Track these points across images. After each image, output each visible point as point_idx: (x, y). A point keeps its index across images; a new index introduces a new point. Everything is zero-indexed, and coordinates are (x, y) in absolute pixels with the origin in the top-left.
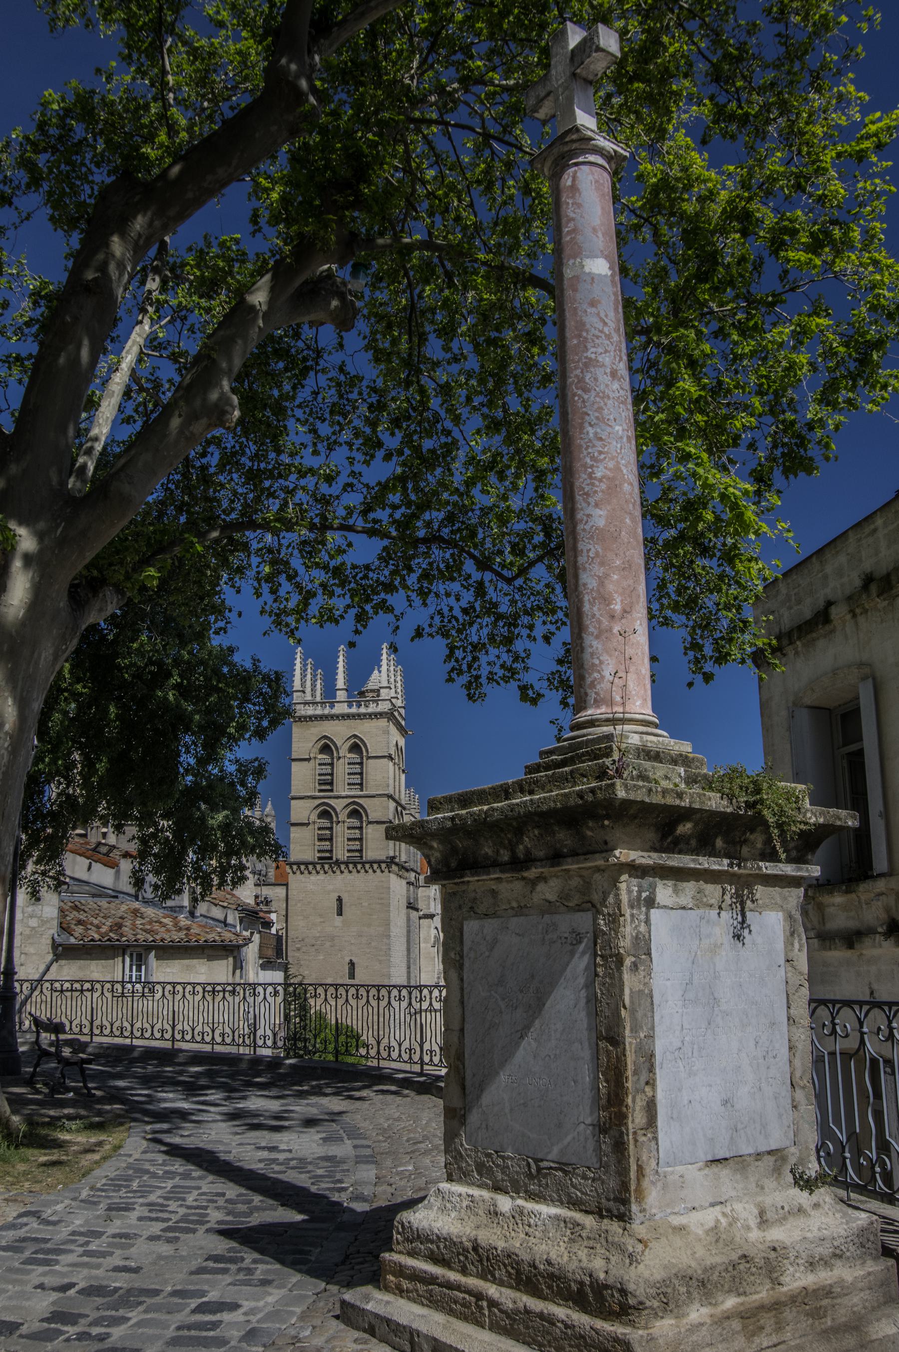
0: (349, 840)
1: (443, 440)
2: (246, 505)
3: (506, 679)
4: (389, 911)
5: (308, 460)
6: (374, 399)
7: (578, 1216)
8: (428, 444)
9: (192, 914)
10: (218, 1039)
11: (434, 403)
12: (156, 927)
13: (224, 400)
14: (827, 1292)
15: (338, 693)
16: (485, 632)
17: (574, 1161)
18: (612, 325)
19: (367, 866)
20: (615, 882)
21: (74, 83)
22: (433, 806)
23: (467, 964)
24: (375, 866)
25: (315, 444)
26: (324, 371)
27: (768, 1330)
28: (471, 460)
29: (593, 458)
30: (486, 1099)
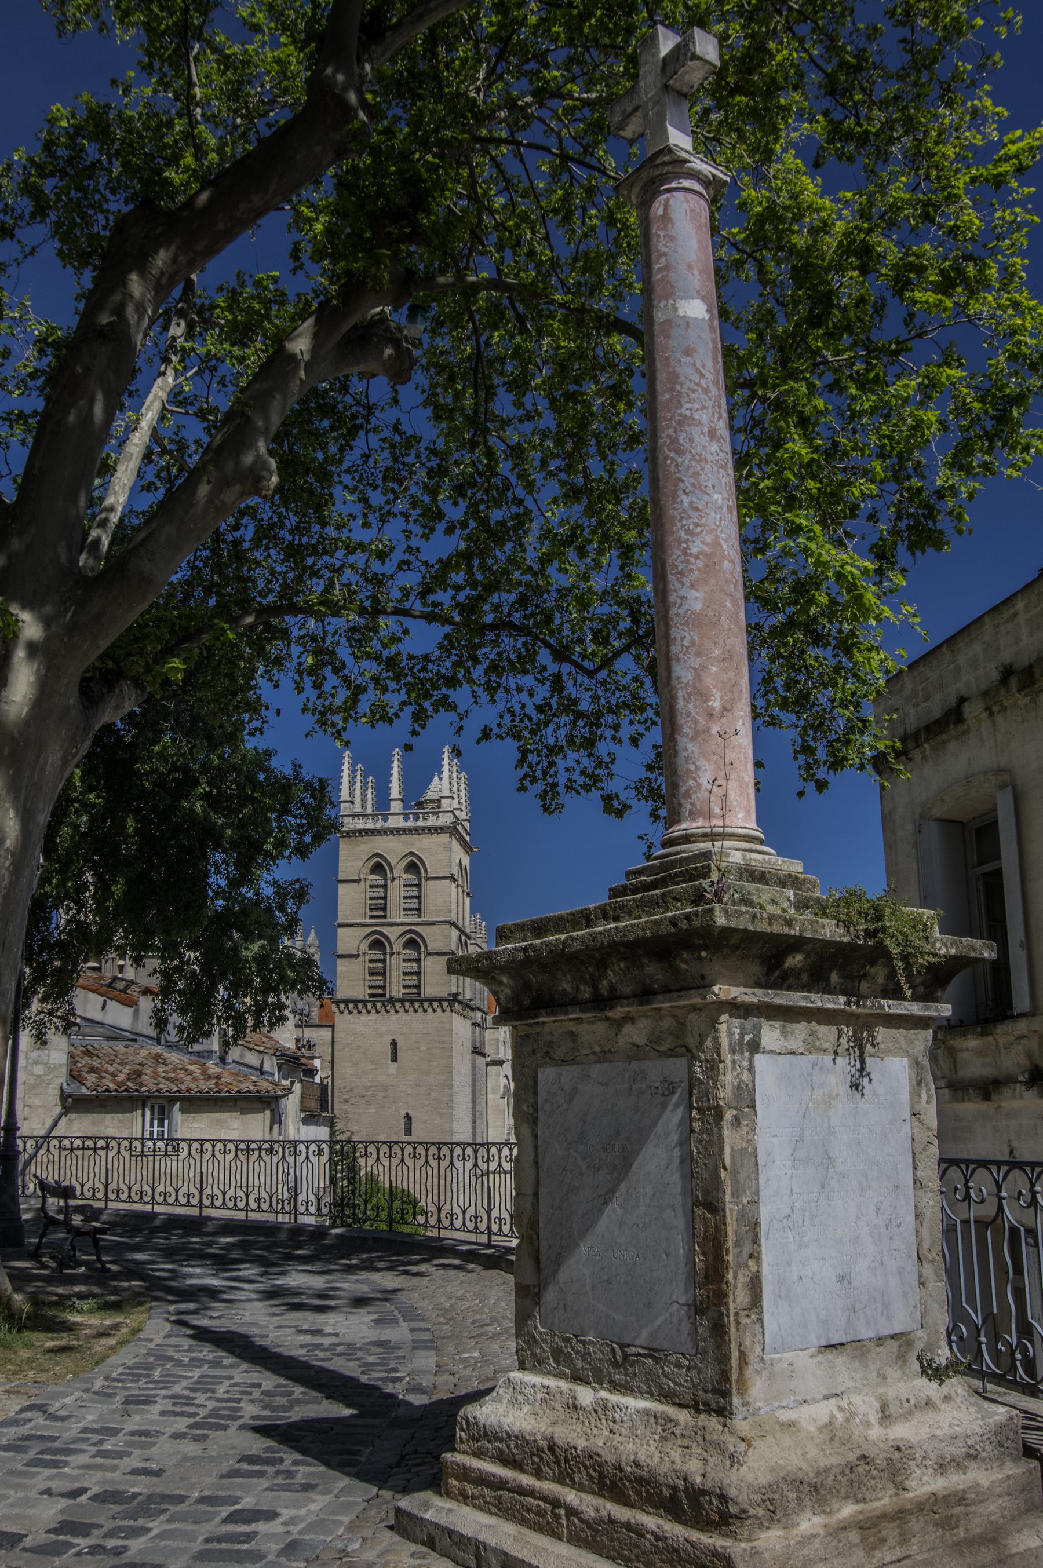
0: (405, 974)
1: (514, 510)
2: (285, 586)
4: (451, 1057)
5: (358, 534)
6: (434, 463)
7: (670, 1410)
8: (496, 515)
9: (223, 1060)
10: (253, 1205)
11: (504, 467)
12: (181, 1075)
13: (260, 463)
14: (959, 1498)
15: (393, 803)
16: (563, 732)
17: (665, 1346)
18: (710, 377)
19: (426, 1004)
20: (713, 1023)
22: (502, 935)
23: (542, 1118)
24: (435, 1004)
25: (365, 515)
26: (376, 430)
27: (891, 1542)
28: (547, 534)
29: (688, 532)
30: (564, 1275)
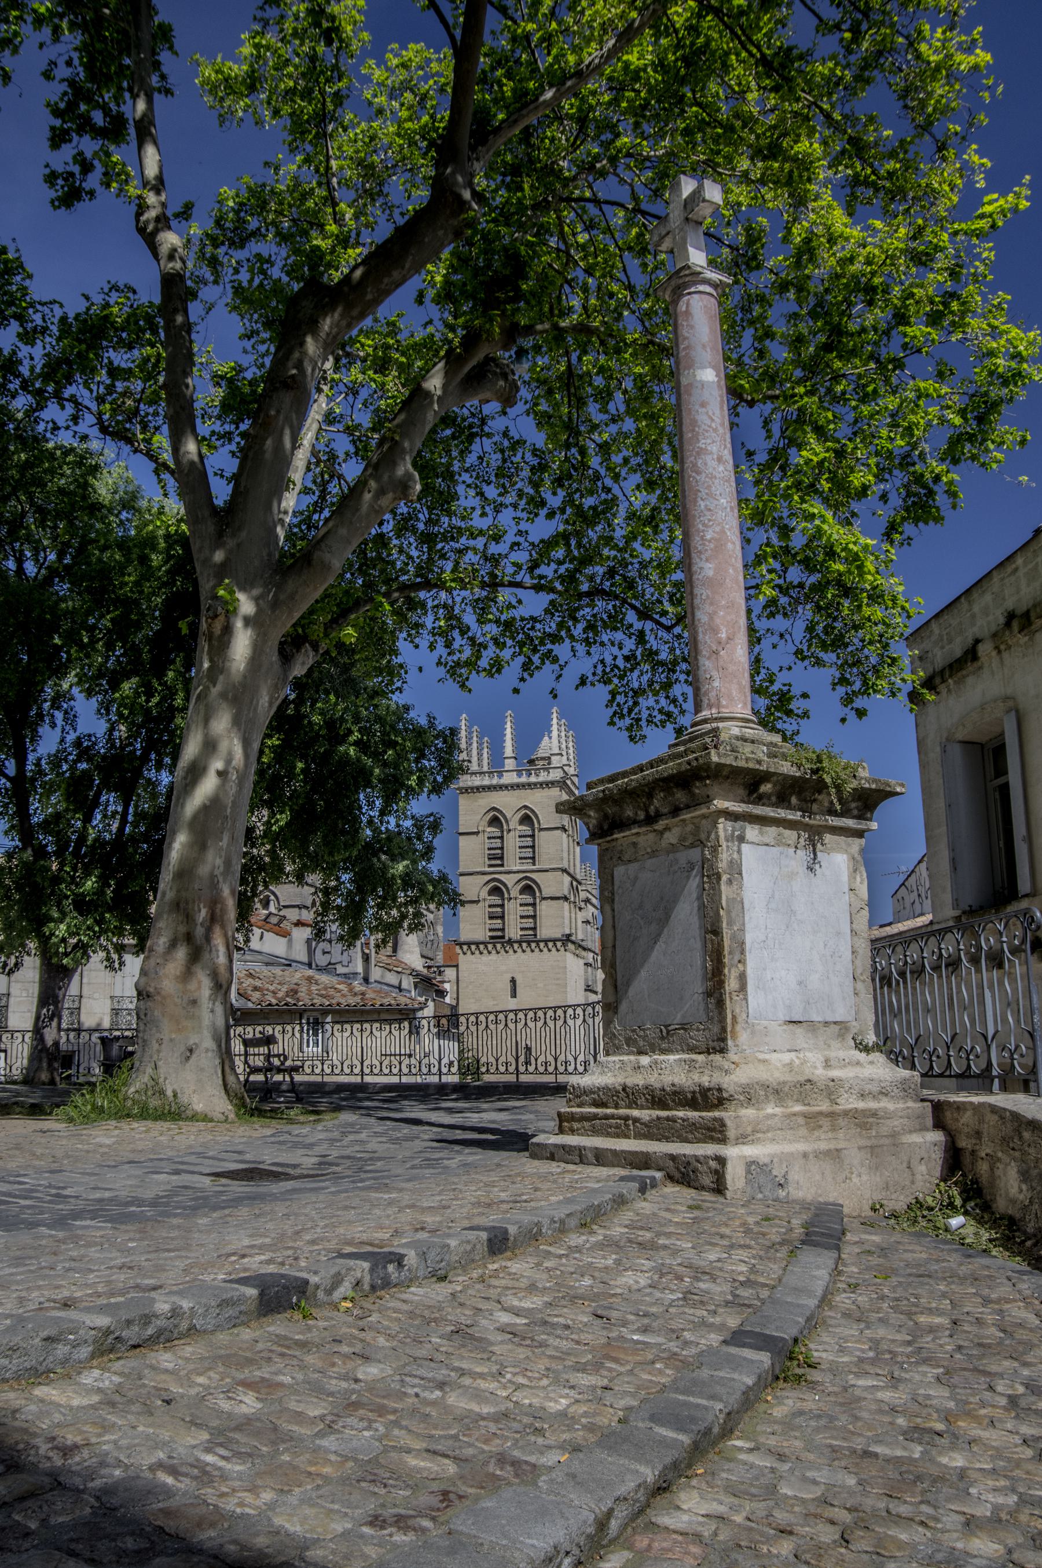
0: (522, 917)
1: (604, 496)
2: (419, 568)
3: (663, 724)
4: (566, 992)
5: (478, 522)
6: (535, 462)
7: (694, 1056)
8: (589, 502)
9: (366, 980)
10: (405, 1070)
11: (594, 461)
12: (332, 992)
13: (409, 476)
14: (874, 1114)
15: (507, 761)
16: (645, 678)
17: (691, 1020)
18: (718, 421)
19: (542, 945)
20: (716, 823)
21: (246, 179)
22: (589, 786)
23: (617, 899)
24: (550, 944)
25: (483, 507)
26: (489, 435)
27: (825, 1128)
28: (632, 516)
29: (704, 525)
30: (631, 992)
